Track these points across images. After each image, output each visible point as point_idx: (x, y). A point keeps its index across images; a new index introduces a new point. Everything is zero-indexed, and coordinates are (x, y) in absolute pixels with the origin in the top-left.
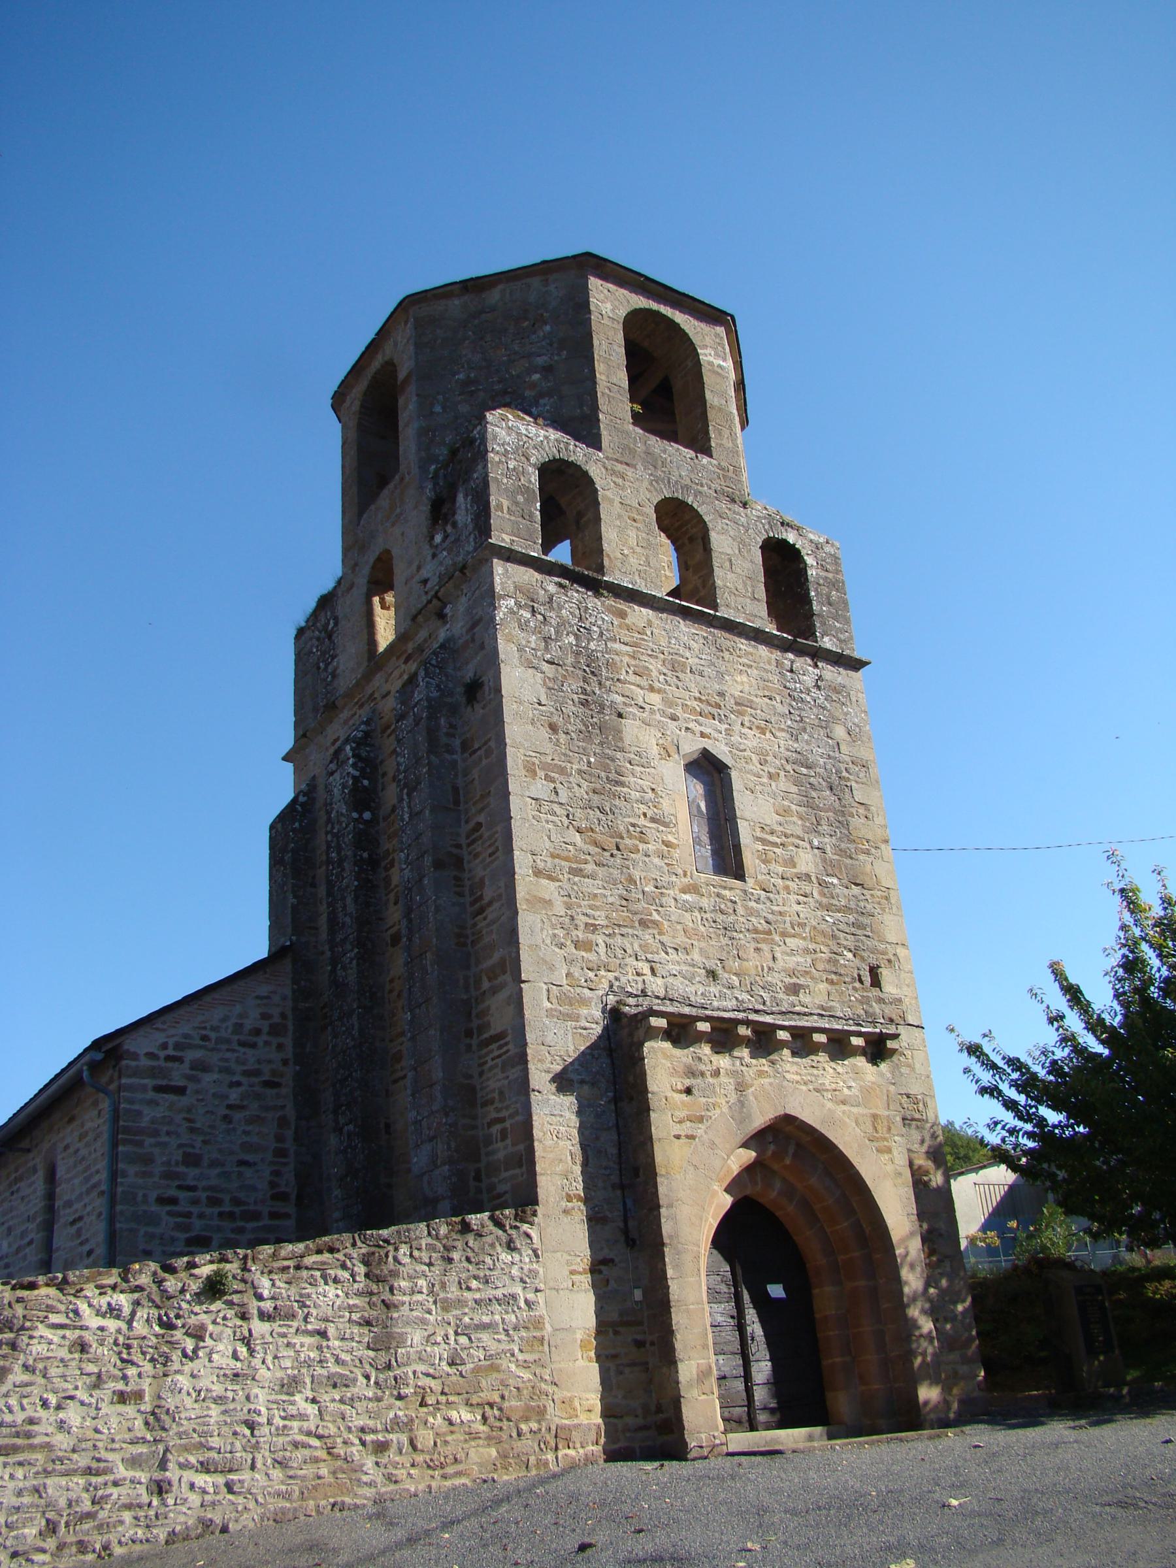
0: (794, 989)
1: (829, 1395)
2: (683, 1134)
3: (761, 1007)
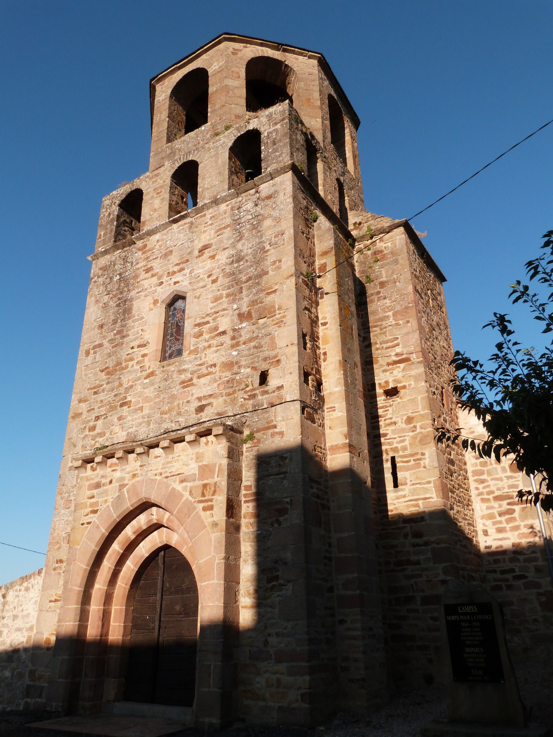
0: (200, 409)
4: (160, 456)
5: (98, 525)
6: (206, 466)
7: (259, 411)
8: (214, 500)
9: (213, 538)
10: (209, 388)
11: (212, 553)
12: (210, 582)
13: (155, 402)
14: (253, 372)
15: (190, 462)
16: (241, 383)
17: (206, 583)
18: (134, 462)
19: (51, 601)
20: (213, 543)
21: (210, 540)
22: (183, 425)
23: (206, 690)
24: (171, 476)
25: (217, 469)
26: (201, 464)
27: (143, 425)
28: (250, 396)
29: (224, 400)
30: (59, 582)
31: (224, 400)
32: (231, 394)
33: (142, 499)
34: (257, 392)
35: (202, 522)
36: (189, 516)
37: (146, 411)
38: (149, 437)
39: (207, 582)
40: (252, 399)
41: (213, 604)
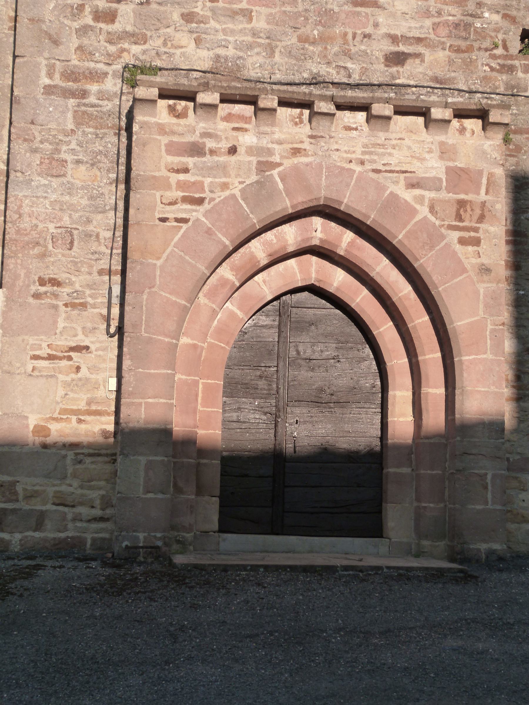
0: (397, 59)
1: (383, 504)
2: (171, 216)
3: (345, 80)
4: (356, 129)
5: (210, 229)
6: (461, 169)
7: (520, 98)
8: (481, 231)
9: (482, 291)
10: (413, 24)
11: (481, 313)
12: (478, 357)
13: (285, 12)
14: (505, 24)
15: (427, 156)
16: (484, 38)
17: (471, 357)
18: (290, 124)
19: (36, 357)
20: (481, 297)
21: (477, 292)
22: (356, 78)
23: (479, 507)
24: (386, 171)
25: (484, 181)
26: (451, 164)
27: (256, 50)
28: (503, 66)
29: (449, 57)
30: (55, 322)
31: (449, 57)
32: (463, 52)
33: (318, 199)
34: (516, 63)
35: (460, 261)
36: (432, 248)
37: (260, 23)
38: (274, 78)
39: (474, 357)
40: (507, 72)
41: (486, 389)
